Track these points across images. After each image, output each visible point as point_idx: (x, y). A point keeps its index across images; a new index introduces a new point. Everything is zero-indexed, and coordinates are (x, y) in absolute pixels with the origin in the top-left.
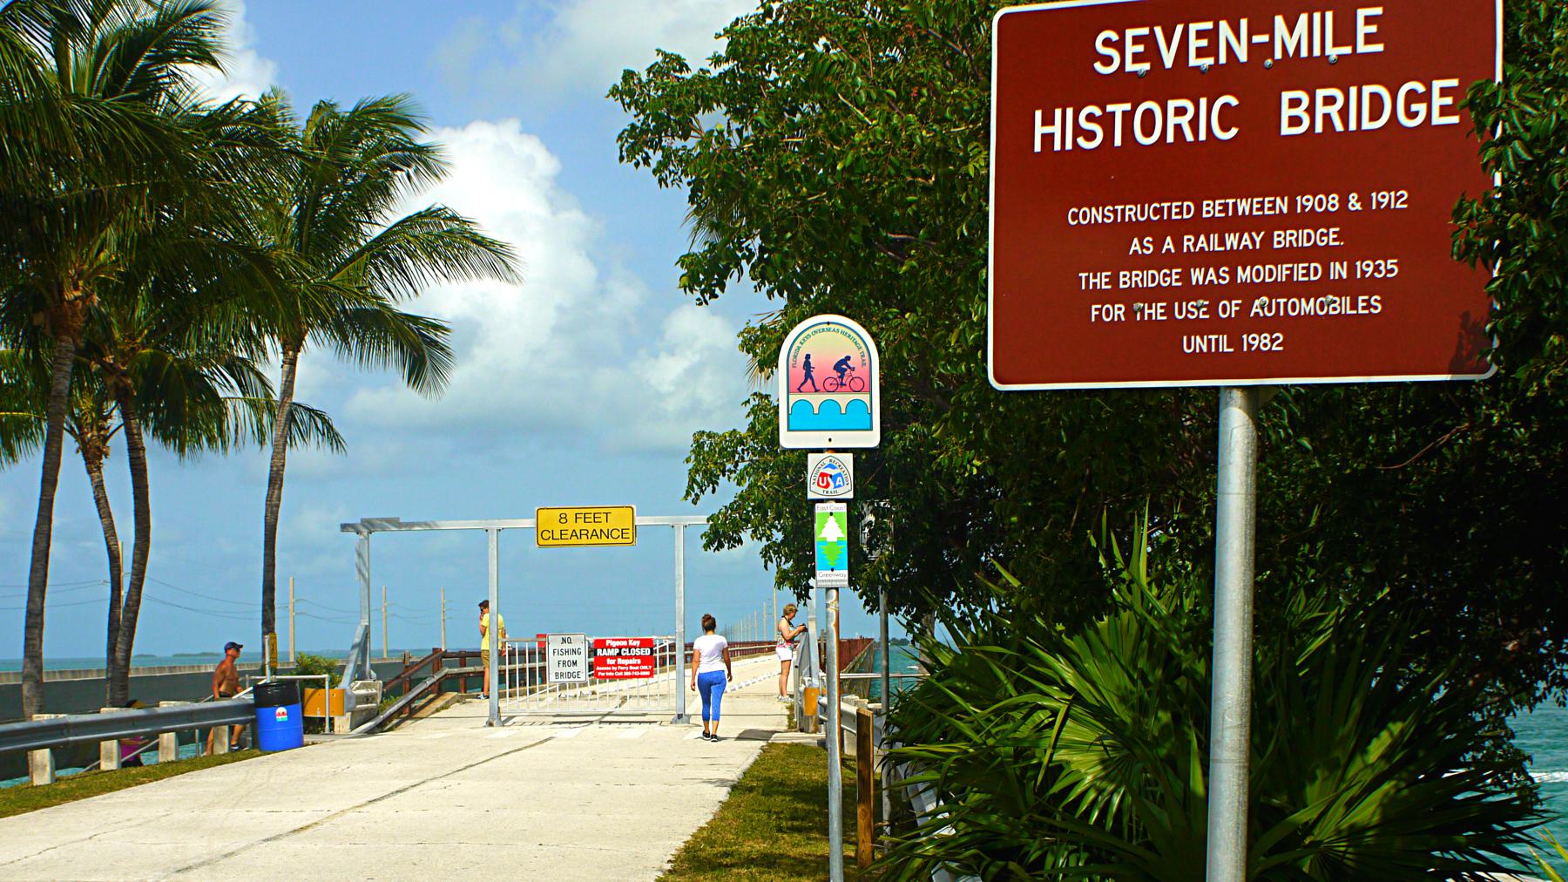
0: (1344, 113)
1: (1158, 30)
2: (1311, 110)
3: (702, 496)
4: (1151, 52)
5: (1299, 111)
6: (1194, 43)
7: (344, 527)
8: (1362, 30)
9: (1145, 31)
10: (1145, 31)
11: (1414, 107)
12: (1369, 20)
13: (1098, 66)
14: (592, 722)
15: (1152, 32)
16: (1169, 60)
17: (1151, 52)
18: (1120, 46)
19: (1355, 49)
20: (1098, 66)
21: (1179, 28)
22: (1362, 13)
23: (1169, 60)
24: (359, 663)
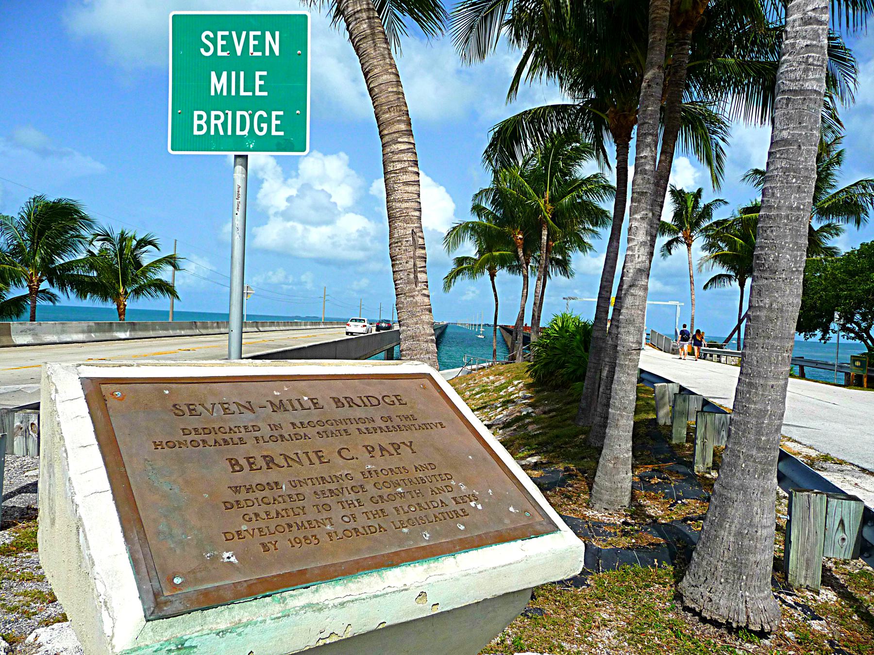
0: (224, 125)
1: (234, 33)
2: (208, 122)
3: (483, 323)
4: (229, 46)
5: (202, 122)
6: (252, 43)
7: (564, 298)
8: (258, 82)
9: (227, 33)
10: (227, 33)
11: (262, 125)
12: (261, 78)
13: (202, 50)
14: (132, 366)
15: (230, 34)
16: (239, 50)
17: (229, 46)
18: (214, 41)
19: (254, 93)
20: (202, 50)
21: (244, 33)
22: (258, 74)
23: (239, 50)
24: (52, 517)
